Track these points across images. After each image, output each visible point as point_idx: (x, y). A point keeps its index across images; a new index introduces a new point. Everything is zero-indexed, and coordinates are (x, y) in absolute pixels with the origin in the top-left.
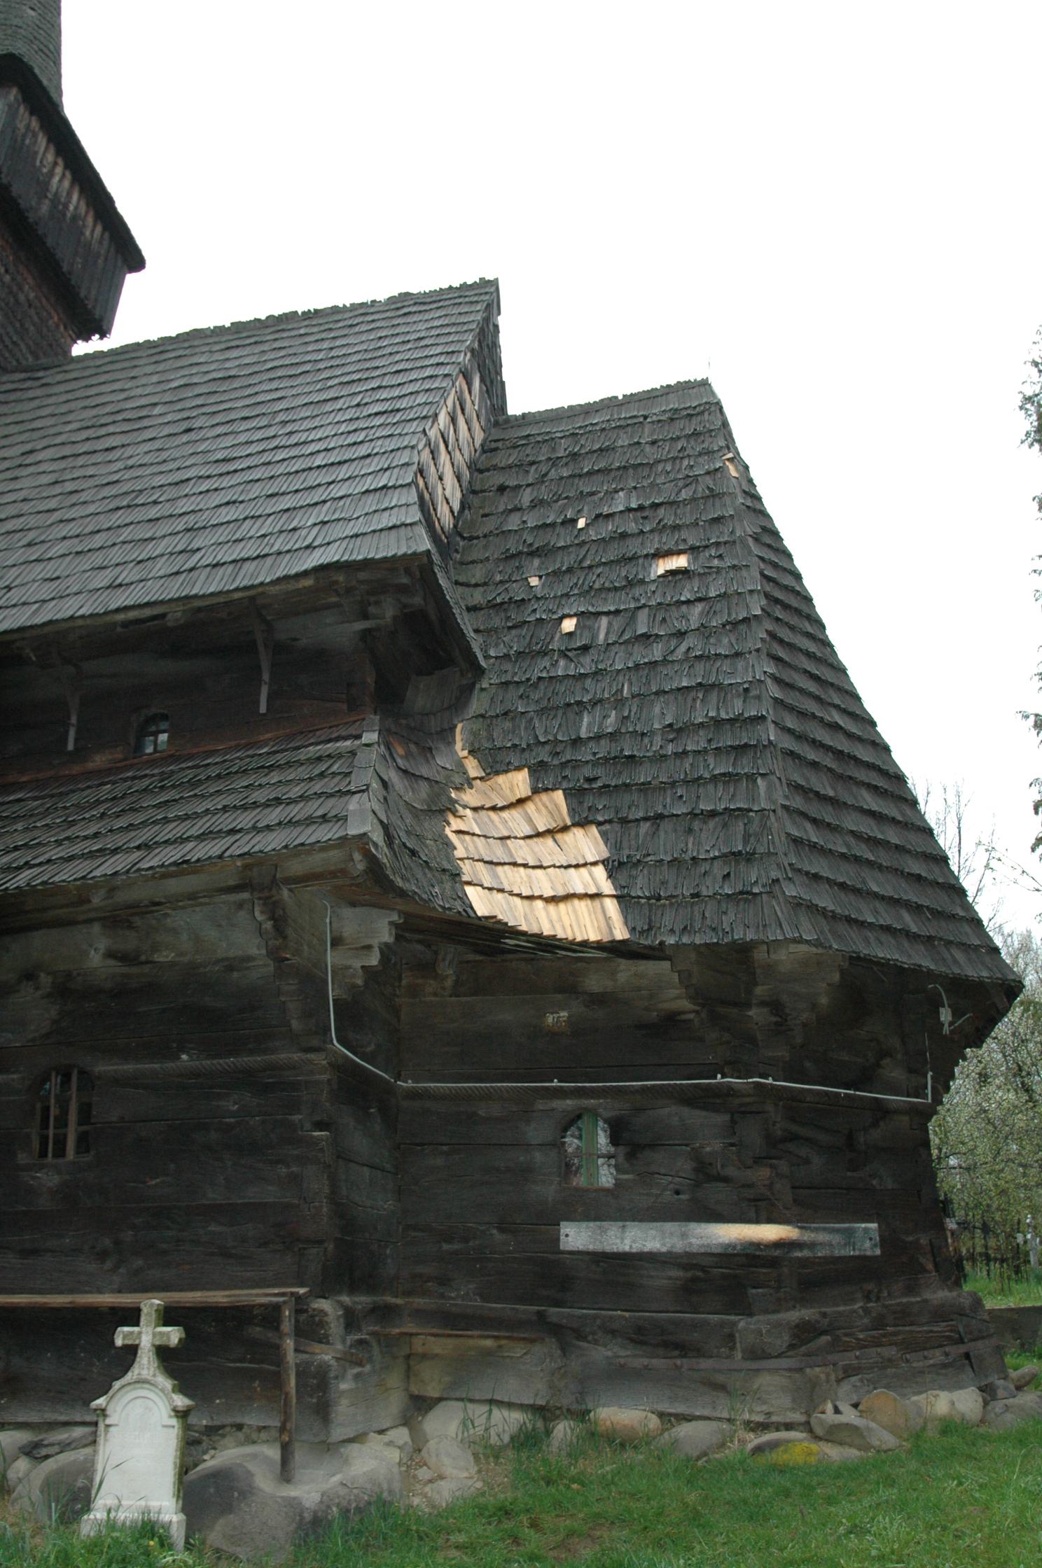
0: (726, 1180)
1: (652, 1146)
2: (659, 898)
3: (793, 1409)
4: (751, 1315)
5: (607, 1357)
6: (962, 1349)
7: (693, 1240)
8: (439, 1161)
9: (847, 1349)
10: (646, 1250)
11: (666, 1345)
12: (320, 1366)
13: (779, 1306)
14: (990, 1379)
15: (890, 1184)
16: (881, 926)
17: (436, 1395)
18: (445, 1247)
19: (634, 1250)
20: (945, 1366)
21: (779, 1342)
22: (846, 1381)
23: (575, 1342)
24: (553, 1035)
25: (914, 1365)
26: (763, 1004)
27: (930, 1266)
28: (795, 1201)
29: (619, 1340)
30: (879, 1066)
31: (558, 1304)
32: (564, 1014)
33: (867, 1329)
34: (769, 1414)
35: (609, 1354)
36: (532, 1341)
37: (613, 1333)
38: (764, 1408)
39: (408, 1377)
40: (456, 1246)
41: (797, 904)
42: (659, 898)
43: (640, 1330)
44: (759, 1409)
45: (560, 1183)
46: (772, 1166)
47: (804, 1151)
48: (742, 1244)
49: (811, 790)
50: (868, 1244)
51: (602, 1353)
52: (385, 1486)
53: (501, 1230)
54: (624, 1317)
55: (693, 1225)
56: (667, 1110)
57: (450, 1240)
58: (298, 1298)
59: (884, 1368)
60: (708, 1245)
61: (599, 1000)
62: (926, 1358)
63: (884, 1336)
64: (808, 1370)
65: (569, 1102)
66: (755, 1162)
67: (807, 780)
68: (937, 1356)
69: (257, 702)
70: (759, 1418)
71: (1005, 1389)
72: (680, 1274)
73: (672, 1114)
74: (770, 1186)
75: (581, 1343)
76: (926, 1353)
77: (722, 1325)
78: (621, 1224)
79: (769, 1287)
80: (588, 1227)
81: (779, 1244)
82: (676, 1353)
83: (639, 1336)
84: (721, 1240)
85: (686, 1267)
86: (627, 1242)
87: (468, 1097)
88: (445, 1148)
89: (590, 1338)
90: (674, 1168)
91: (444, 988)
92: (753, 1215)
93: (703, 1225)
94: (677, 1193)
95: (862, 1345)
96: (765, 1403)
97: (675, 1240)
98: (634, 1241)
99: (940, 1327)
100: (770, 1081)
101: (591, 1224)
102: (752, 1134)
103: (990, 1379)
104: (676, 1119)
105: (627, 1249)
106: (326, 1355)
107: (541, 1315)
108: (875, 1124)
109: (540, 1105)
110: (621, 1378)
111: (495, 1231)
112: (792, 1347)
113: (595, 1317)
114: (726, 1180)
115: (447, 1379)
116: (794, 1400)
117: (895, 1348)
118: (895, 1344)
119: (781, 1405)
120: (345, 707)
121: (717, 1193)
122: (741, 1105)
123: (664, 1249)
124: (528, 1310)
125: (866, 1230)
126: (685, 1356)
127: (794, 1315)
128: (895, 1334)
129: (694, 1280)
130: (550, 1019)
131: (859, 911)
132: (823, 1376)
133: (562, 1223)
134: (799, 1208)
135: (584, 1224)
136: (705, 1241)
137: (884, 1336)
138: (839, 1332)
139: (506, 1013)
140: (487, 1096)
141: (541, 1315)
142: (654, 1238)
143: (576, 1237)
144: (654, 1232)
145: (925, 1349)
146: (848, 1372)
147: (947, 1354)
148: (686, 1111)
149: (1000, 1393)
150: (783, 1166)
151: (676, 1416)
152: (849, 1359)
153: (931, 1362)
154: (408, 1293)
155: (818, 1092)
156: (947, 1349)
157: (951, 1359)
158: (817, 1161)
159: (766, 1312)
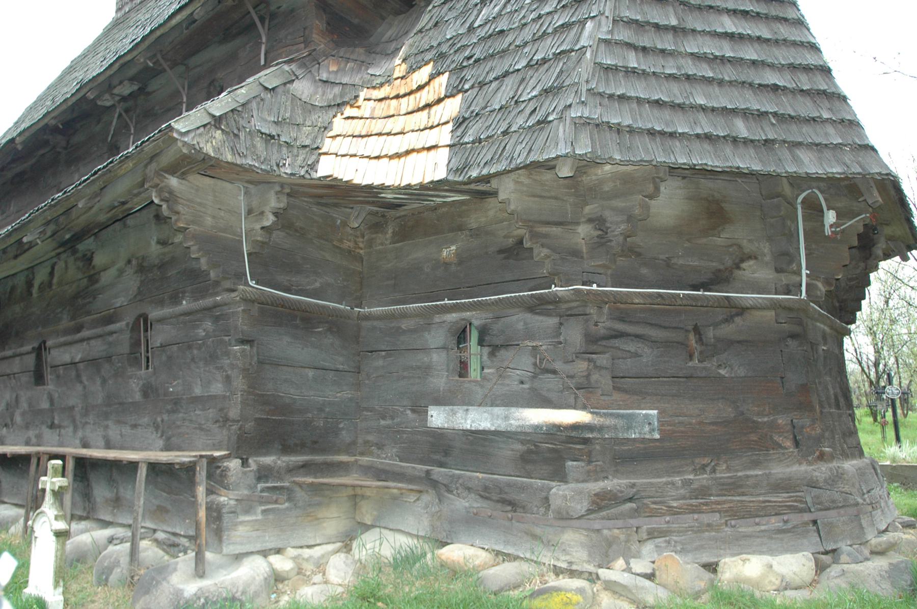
0: (554, 372)
1: (506, 346)
2: (480, 141)
3: (589, 562)
4: (566, 482)
5: (466, 508)
6: (807, 517)
7: (512, 422)
8: (380, 363)
9: (653, 514)
10: (481, 428)
11: (504, 502)
12: (217, 505)
13: (591, 476)
14: (839, 545)
15: (742, 372)
16: (698, 136)
17: (369, 523)
18: (383, 422)
19: (473, 429)
20: (780, 531)
21: (579, 507)
22: (650, 542)
23: (446, 494)
24: (447, 264)
25: (740, 530)
26: (590, 221)
27: (788, 443)
28: (614, 388)
29: (473, 495)
30: (738, 268)
31: (441, 465)
32: (453, 248)
33: (684, 498)
34: (571, 563)
35: (467, 504)
36: (420, 492)
37: (469, 489)
38: (568, 558)
39: (355, 509)
40: (388, 422)
41: (582, 124)
42: (480, 141)
43: (486, 489)
44: (563, 558)
45: (448, 376)
46: (590, 360)
47: (632, 346)
48: (547, 426)
49: (648, 23)
50: (647, 428)
51: (462, 503)
52: (241, 589)
53: (413, 411)
54: (478, 477)
55: (513, 409)
56: (514, 318)
57: (384, 418)
58: (212, 461)
59: (701, 531)
60: (522, 426)
61: (476, 233)
62: (757, 524)
63: (706, 504)
64: (605, 532)
65: (454, 315)
66: (577, 357)
67: (645, 14)
68: (775, 522)
69: (260, 60)
70: (564, 565)
71: (849, 554)
72: (519, 447)
73: (519, 320)
74: (588, 377)
75: (450, 496)
76: (757, 520)
77: (542, 489)
78: (465, 407)
79: (582, 460)
80: (444, 410)
81: (576, 427)
82: (509, 508)
83: (485, 492)
84: (532, 422)
85: (522, 442)
86: (469, 422)
87: (391, 317)
88: (383, 353)
89: (455, 492)
90: (520, 364)
91: (386, 239)
92: (572, 400)
93: (521, 410)
94: (522, 383)
95: (672, 511)
96: (568, 554)
97: (499, 422)
98: (473, 422)
99: (782, 497)
100: (595, 287)
101: (447, 408)
102: (574, 334)
103: (839, 545)
104: (522, 323)
105: (469, 427)
106: (224, 499)
107: (428, 472)
108: (728, 320)
109: (437, 319)
110: (471, 523)
111: (409, 412)
112: (590, 511)
113: (459, 477)
114: (554, 372)
115: (375, 513)
116: (590, 555)
117: (718, 515)
118: (719, 511)
119: (580, 557)
120: (302, 45)
121: (549, 383)
122: (568, 309)
123: (493, 429)
124: (421, 468)
125: (646, 415)
126: (515, 511)
127: (596, 486)
128: (718, 503)
129: (529, 452)
130: (445, 253)
131: (826, 134)
132: (622, 537)
133: (430, 408)
134: (579, 393)
135: (442, 408)
136: (521, 423)
137: (706, 504)
138: (646, 501)
139: (418, 252)
140: (404, 315)
141: (428, 472)
142: (486, 419)
143: (437, 417)
144: (486, 415)
145: (758, 516)
146: (652, 535)
147: (786, 522)
148: (528, 316)
149: (844, 558)
150: (603, 360)
151: (508, 555)
152: (647, 524)
153: (763, 528)
154: (362, 454)
155: (650, 295)
156: (785, 518)
157: (789, 526)
158: (648, 354)
159: (578, 481)
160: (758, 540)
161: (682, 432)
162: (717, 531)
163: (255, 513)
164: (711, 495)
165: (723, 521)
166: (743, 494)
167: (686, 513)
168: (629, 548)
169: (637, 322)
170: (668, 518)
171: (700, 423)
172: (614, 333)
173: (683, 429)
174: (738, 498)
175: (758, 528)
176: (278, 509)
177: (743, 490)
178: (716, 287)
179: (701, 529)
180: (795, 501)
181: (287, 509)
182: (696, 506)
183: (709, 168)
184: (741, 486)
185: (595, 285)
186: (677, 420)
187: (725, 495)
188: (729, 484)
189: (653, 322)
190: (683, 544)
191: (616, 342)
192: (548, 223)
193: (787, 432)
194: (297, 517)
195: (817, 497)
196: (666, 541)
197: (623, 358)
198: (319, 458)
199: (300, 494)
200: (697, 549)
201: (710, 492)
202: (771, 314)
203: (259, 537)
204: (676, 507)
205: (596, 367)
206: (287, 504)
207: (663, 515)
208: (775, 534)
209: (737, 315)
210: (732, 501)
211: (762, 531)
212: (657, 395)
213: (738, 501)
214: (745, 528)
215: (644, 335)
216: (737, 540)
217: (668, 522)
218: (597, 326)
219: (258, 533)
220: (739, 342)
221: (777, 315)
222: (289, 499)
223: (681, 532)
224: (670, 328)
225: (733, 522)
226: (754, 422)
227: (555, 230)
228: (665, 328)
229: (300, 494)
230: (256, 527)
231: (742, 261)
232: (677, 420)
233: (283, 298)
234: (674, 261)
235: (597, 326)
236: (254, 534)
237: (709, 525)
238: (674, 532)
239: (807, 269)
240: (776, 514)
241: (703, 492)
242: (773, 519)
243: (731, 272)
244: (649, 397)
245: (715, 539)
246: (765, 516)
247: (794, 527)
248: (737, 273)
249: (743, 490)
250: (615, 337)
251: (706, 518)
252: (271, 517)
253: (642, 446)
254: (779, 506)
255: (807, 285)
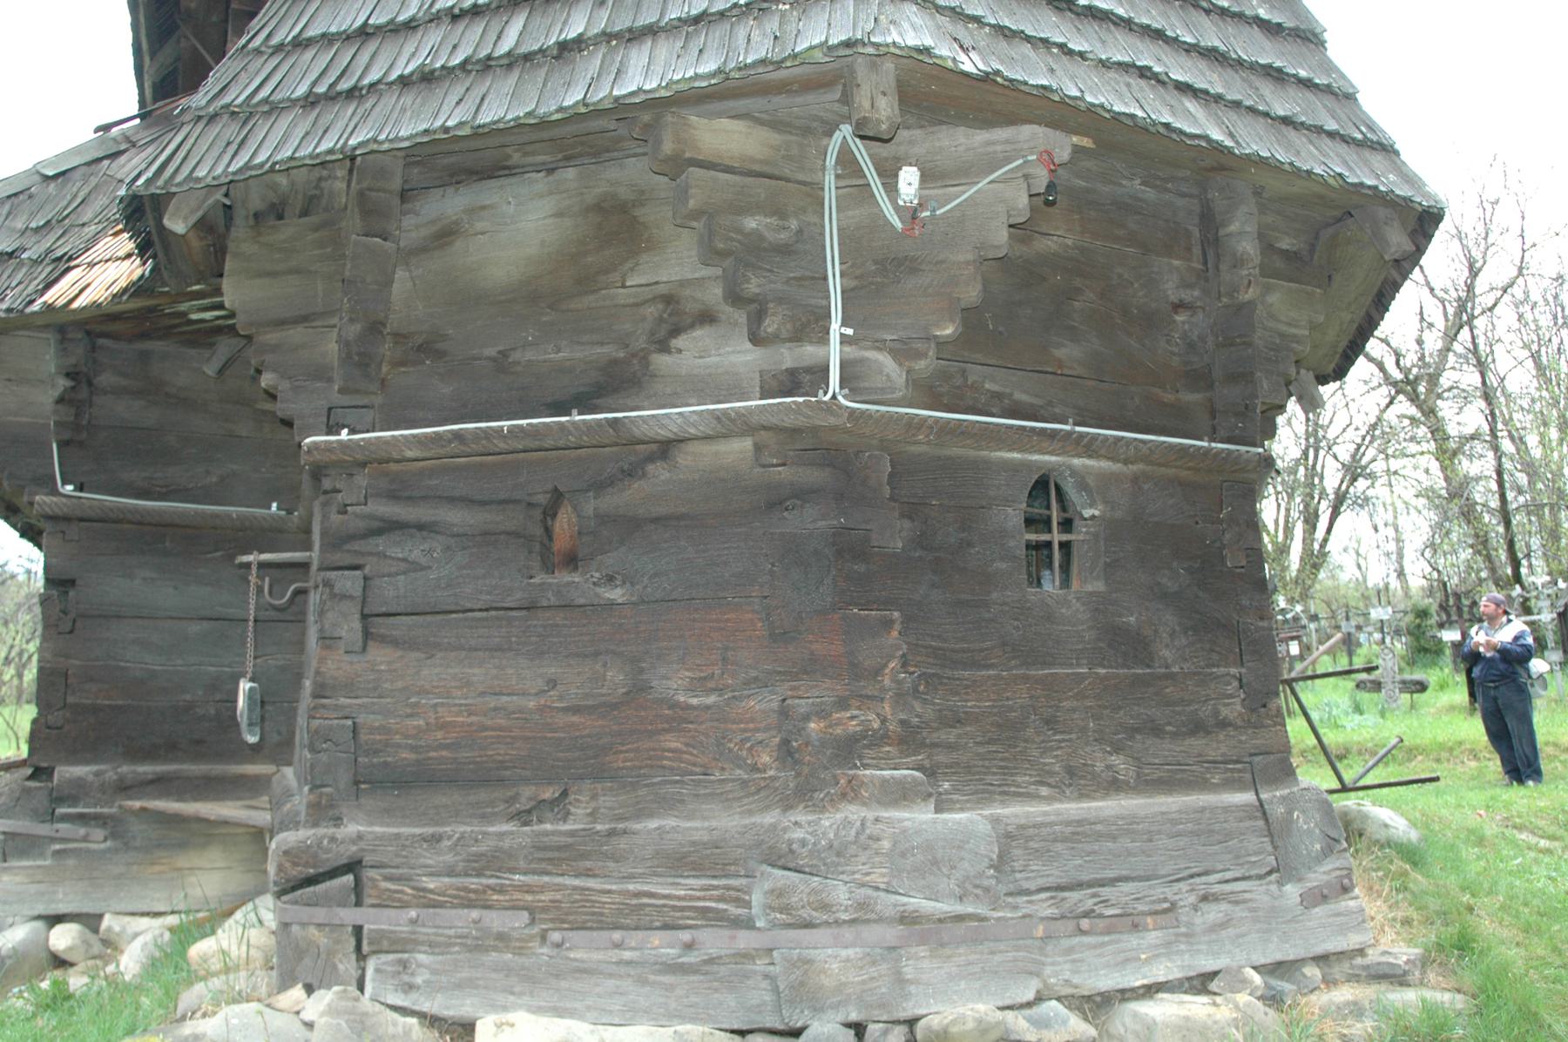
33: (451, 873)
47: (414, 549)
59: (479, 948)
62: (618, 946)
63: (501, 890)
68: (662, 945)
76: (617, 935)
95: (428, 901)
99: (686, 887)
100: (344, 435)
128: (528, 889)
137: (501, 890)
145: (616, 927)
153: (627, 955)
156: (685, 936)
160: (611, 983)
161: (501, 729)
162: (519, 951)
163: (42, 855)
164: (513, 871)
165: (536, 930)
166: (589, 873)
167: (454, 907)
168: (335, 967)
169: (424, 498)
170: (413, 913)
171: (541, 709)
172: (376, 524)
173: (502, 722)
174: (577, 882)
175: (614, 955)
176: (88, 851)
177: (588, 864)
178: (629, 402)
179: (479, 944)
180: (720, 899)
181: (109, 850)
182: (475, 891)
183: (386, 146)
184: (584, 856)
185: (345, 431)
186: (492, 702)
187: (547, 873)
188: (559, 848)
189: (457, 493)
190: (434, 972)
191: (380, 543)
192: (281, 323)
193: (767, 729)
194: (128, 864)
195: (778, 893)
196: (400, 961)
197: (389, 575)
198: (218, 769)
199: (136, 827)
200: (459, 986)
201: (512, 864)
202: (742, 446)
203: (43, 894)
204: (431, 891)
205: (333, 596)
206: (108, 843)
207: (405, 905)
208: (660, 972)
209: (651, 458)
210: (559, 888)
211: (629, 963)
212: (461, 648)
213: (575, 888)
214: (585, 949)
215: (435, 523)
216: (557, 976)
217: (414, 922)
218: (346, 512)
219: (42, 887)
220: (656, 520)
221: (758, 448)
222: (114, 835)
223: (438, 945)
224: (491, 503)
225: (556, 936)
226: (674, 705)
227: (296, 334)
228: (483, 503)
229: (136, 827)
230: (39, 877)
231: (676, 331)
232: (492, 702)
233: (136, 510)
234: (516, 356)
235: (346, 512)
236: (33, 888)
237: (501, 937)
238: (423, 943)
239: (845, 323)
240: (666, 927)
241: (493, 862)
242: (656, 938)
243: (645, 362)
244: (439, 655)
245: (508, 970)
246: (637, 928)
247: (705, 962)
248: (661, 361)
249: (588, 864)
250: (379, 532)
251: (496, 921)
252: (71, 862)
253: (413, 756)
254: (674, 908)
255: (844, 365)
